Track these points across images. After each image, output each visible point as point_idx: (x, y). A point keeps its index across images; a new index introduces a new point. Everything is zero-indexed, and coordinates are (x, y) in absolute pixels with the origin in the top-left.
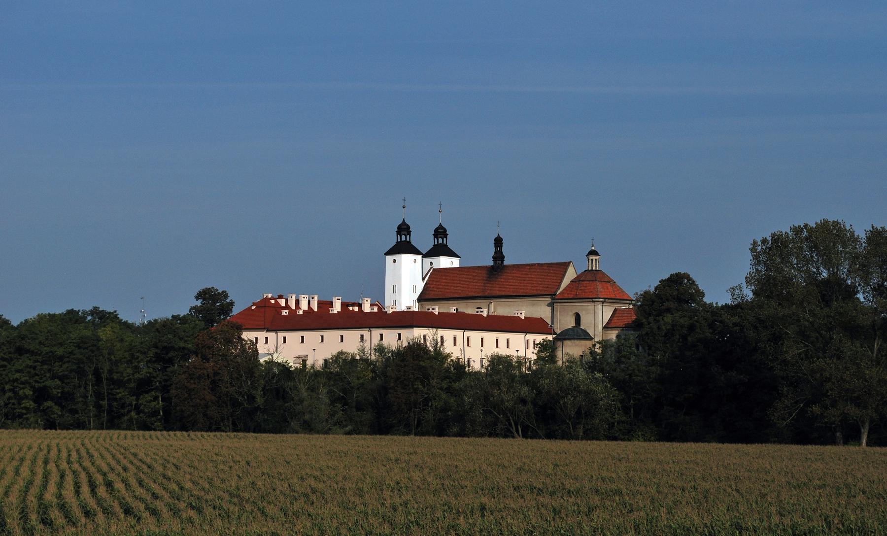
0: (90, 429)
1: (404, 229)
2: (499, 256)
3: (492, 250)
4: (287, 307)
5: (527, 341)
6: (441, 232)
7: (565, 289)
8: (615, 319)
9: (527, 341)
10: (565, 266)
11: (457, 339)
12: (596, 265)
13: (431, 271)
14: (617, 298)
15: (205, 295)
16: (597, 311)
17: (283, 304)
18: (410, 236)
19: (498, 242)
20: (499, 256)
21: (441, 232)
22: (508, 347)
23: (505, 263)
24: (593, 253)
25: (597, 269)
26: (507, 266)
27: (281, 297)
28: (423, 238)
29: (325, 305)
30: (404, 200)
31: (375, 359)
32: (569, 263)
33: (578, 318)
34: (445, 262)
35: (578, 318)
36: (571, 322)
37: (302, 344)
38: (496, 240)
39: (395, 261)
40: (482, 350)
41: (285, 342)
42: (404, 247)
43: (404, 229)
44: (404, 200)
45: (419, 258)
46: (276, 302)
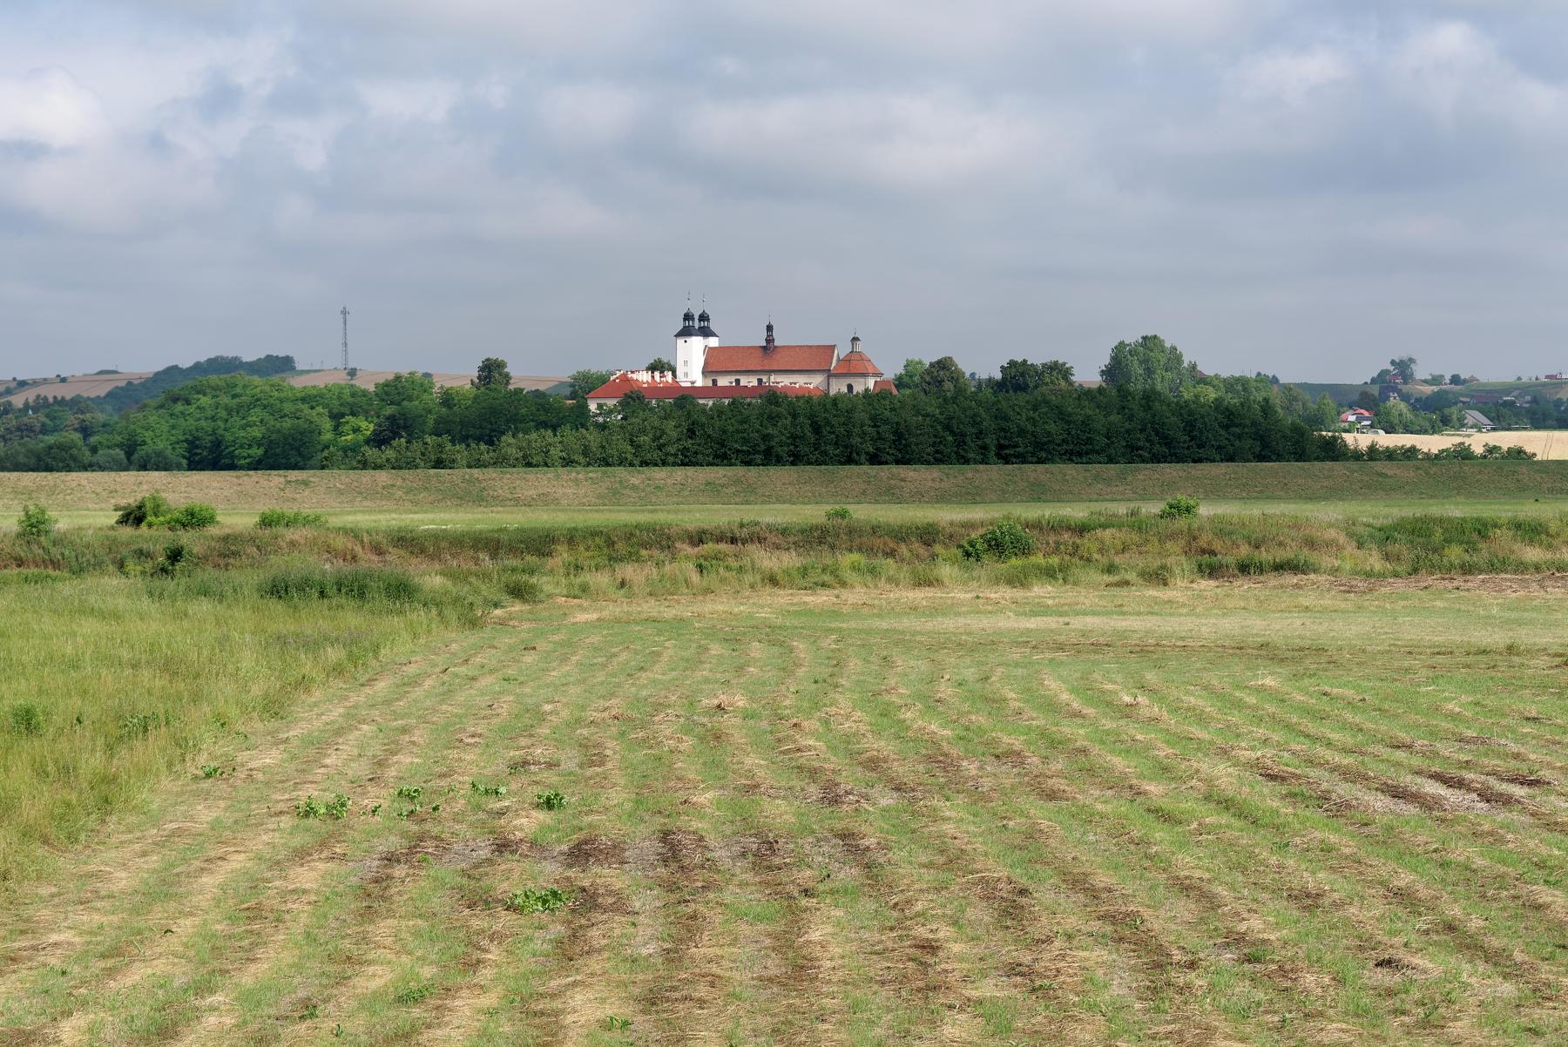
2: (770, 340)
19: (770, 328)
20: (770, 340)
23: (776, 344)
34: (713, 342)
42: (686, 332)
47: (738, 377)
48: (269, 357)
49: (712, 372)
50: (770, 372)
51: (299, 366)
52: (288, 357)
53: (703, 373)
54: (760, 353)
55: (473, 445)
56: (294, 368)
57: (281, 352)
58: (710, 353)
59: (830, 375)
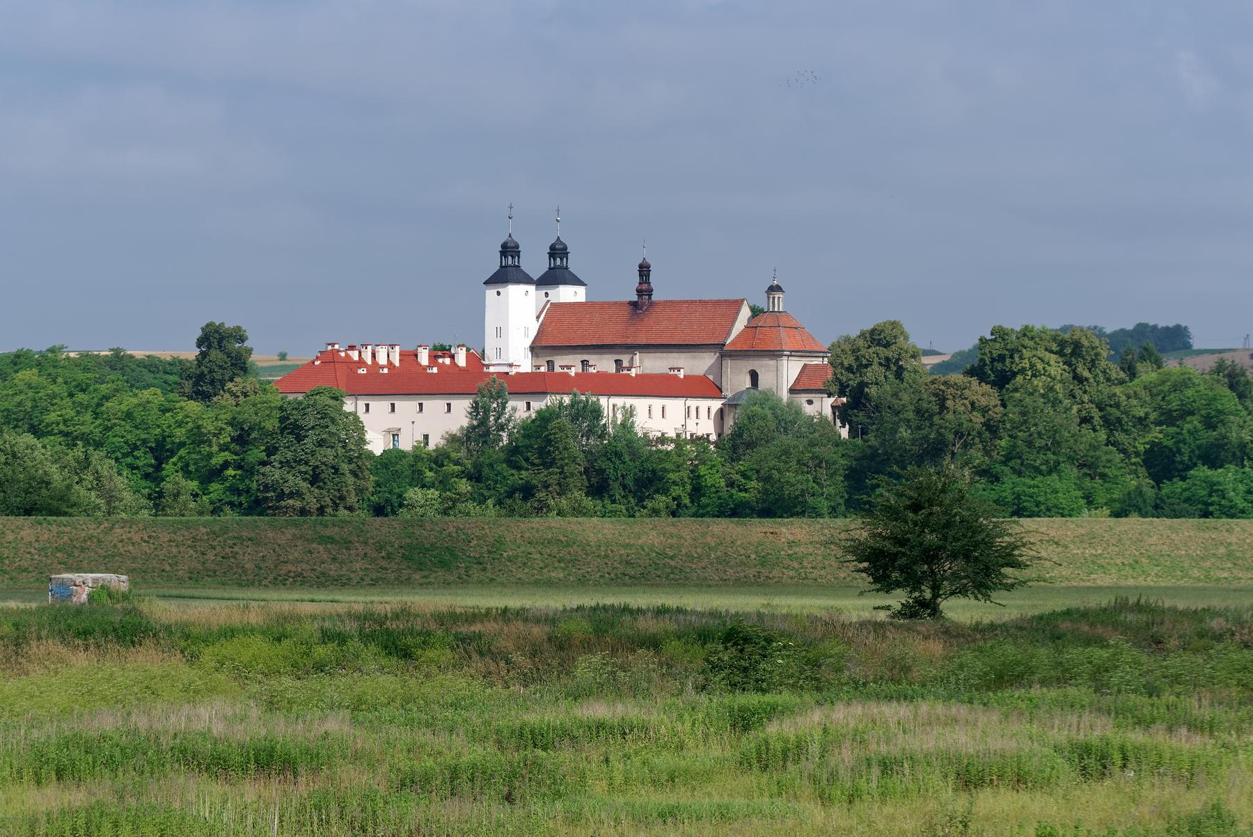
0: (387, 515)
1: (509, 249)
2: (644, 291)
3: (635, 280)
4: (361, 362)
5: (688, 408)
6: (558, 251)
7: (738, 337)
8: (804, 378)
9: (688, 408)
10: (738, 304)
11: (700, 410)
12: (779, 304)
13: (548, 306)
14: (806, 349)
15: (212, 338)
16: (780, 368)
17: (356, 358)
18: (519, 257)
19: (644, 270)
20: (644, 291)
21: (558, 251)
22: (663, 417)
23: (654, 298)
24: (778, 289)
25: (781, 310)
26: (656, 303)
27: (352, 348)
28: (535, 261)
29: (410, 356)
30: (511, 207)
31: (913, 442)
32: (742, 301)
33: (754, 376)
34: (568, 294)
35: (754, 376)
36: (745, 383)
37: (392, 414)
38: (641, 266)
39: (499, 293)
40: (697, 424)
41: (367, 410)
42: (506, 275)
43: (509, 249)
44: (511, 207)
45: (532, 288)
46: (347, 355)
47: (585, 357)
48: (1122, 330)
49: (546, 347)
50: (631, 348)
51: (1197, 344)
52: (1178, 327)
53: (532, 349)
54: (626, 312)
55: (164, 473)
56: (1187, 346)
57: (1164, 320)
58: (555, 315)
59: (725, 353)
